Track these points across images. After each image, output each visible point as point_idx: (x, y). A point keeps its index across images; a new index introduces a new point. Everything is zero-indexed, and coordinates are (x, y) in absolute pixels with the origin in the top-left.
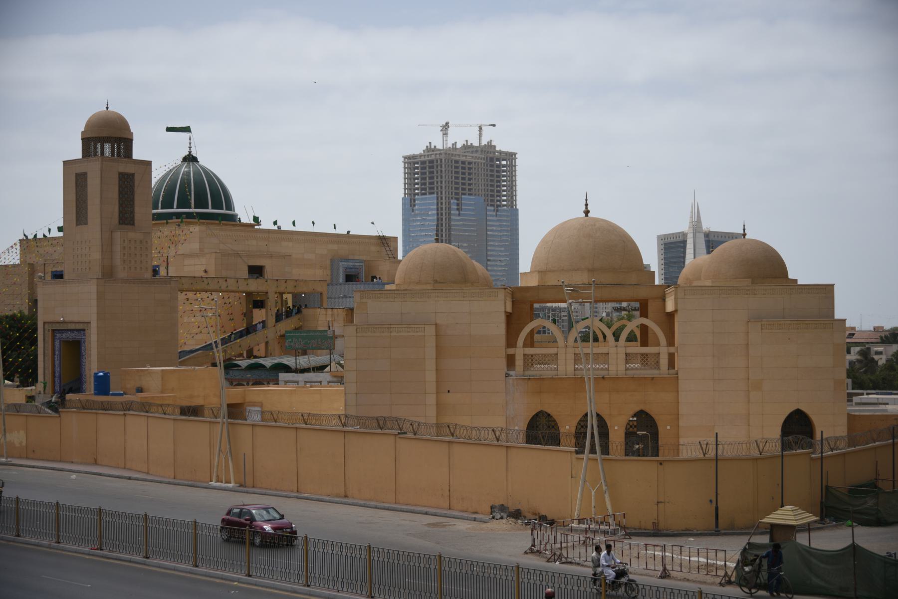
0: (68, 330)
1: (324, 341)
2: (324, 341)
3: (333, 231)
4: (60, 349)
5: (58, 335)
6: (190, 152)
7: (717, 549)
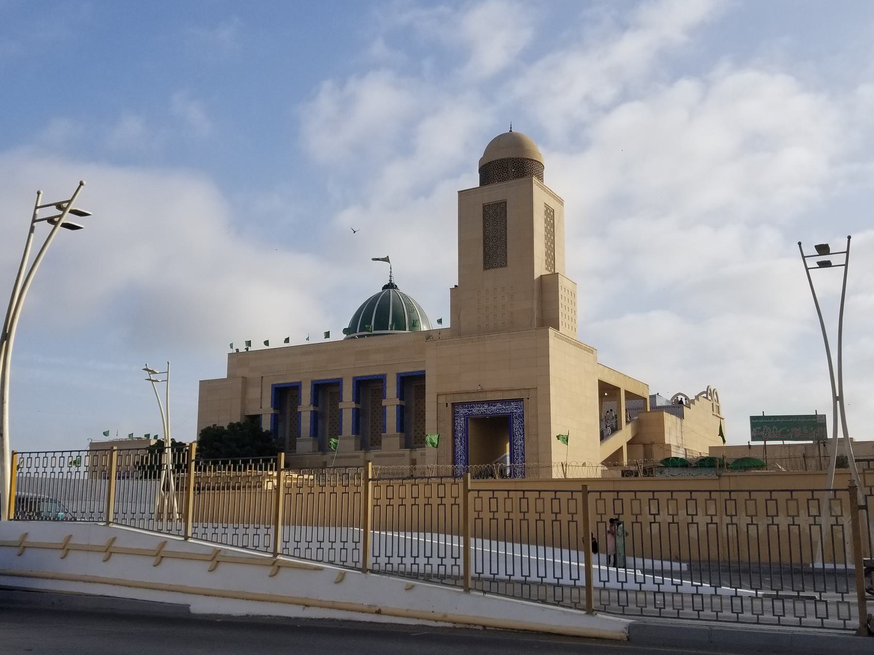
0: (478, 402)
1: (812, 429)
2: (812, 429)
3: (307, 343)
4: (466, 431)
5: (462, 411)
6: (391, 281)
7: (751, 489)
